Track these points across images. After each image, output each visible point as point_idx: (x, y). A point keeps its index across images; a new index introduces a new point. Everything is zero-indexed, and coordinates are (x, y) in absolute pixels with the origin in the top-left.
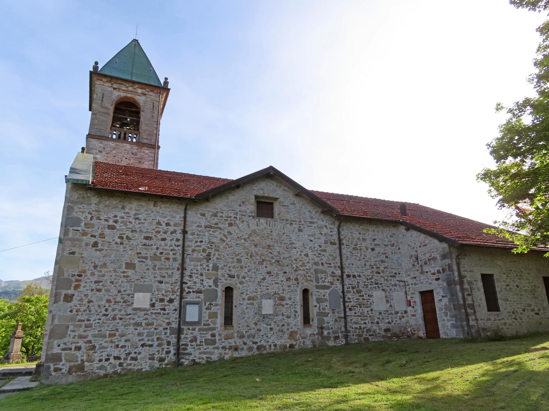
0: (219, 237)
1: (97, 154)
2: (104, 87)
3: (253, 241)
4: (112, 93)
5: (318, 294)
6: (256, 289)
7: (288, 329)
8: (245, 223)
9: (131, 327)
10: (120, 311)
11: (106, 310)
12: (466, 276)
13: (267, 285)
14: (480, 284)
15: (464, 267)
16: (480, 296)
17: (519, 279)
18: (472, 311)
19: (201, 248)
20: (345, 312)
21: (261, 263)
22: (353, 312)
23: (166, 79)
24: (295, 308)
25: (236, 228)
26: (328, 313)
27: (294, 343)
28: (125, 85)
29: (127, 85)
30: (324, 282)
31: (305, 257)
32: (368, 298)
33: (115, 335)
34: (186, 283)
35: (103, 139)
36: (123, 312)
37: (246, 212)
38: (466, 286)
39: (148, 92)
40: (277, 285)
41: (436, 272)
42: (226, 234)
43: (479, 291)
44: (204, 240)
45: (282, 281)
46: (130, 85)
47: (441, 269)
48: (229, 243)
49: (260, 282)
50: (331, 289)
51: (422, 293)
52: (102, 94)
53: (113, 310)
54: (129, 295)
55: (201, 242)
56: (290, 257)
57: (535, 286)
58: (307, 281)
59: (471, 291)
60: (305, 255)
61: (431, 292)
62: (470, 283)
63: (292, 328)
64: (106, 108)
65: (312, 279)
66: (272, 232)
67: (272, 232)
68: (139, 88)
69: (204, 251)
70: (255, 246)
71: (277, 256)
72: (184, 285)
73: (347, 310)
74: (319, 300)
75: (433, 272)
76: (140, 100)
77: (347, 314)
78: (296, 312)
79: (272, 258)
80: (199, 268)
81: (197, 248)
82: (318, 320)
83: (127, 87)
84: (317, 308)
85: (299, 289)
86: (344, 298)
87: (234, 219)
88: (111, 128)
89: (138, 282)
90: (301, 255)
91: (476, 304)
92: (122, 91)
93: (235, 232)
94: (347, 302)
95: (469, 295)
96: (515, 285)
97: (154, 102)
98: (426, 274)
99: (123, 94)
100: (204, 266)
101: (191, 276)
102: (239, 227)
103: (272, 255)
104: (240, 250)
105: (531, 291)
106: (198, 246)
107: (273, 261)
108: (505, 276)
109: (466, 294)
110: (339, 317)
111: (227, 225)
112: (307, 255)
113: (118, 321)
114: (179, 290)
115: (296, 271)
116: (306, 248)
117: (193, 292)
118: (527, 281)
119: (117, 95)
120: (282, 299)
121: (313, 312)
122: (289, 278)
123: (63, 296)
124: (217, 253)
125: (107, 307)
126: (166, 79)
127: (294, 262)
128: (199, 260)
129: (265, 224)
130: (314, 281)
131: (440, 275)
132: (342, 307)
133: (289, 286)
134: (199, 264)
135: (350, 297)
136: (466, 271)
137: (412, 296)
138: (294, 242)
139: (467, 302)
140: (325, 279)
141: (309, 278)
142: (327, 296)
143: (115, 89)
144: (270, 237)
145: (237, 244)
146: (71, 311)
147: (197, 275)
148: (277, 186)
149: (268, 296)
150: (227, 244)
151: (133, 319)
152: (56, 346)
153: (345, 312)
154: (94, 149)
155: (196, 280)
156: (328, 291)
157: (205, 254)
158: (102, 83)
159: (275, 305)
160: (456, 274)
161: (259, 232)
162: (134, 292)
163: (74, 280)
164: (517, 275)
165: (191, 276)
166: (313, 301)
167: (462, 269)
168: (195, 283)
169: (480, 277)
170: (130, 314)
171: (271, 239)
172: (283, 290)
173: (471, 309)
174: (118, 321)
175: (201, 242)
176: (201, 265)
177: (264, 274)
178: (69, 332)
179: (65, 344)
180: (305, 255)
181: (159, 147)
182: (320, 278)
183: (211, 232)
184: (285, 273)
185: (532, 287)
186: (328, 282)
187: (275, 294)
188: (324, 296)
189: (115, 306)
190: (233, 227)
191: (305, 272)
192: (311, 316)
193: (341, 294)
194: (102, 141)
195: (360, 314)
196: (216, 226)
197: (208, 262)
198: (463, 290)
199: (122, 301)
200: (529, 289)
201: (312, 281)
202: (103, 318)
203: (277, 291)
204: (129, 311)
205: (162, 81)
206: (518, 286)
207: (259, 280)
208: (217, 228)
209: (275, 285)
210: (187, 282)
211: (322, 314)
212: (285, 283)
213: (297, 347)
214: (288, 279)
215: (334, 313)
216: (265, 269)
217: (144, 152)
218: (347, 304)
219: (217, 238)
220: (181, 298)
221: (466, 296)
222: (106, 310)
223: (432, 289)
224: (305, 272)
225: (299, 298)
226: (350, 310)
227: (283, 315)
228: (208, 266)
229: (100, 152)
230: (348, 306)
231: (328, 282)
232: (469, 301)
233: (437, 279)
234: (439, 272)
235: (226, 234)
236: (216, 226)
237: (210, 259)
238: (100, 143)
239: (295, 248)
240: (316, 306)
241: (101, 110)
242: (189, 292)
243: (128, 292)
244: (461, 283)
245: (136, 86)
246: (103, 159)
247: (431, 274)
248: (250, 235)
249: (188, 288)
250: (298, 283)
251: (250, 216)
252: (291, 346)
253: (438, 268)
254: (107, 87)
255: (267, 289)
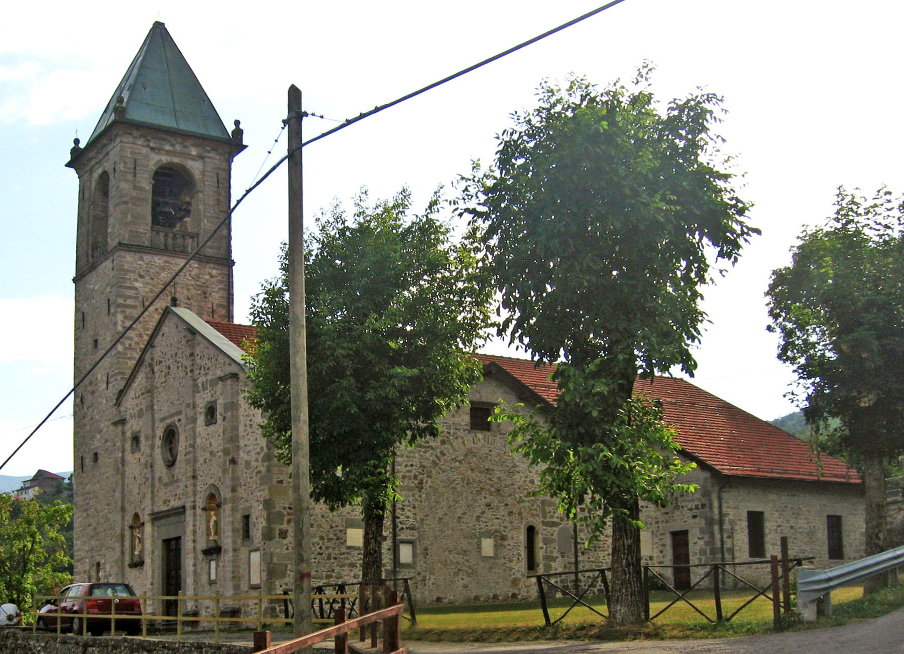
0: (431, 459)
1: (136, 280)
2: (135, 146)
3: (469, 463)
4: (147, 157)
5: (545, 532)
6: (474, 526)
7: (510, 576)
8: (460, 440)
9: (346, 568)
10: (334, 549)
11: (321, 548)
12: (728, 514)
13: (487, 520)
14: (745, 524)
15: (727, 502)
16: (742, 539)
17: (796, 518)
18: (731, 557)
19: (412, 474)
20: (576, 557)
21: (479, 492)
22: (586, 556)
23: (237, 123)
24: (518, 550)
25: (449, 446)
26: (557, 557)
27: (517, 592)
28: (169, 141)
29: (174, 142)
30: (552, 517)
31: (529, 485)
32: (606, 539)
33: (331, 577)
34: (399, 518)
35: (145, 252)
36: (337, 551)
37: (460, 424)
38: (727, 526)
39: (209, 152)
40: (498, 521)
41: (694, 507)
42: (439, 455)
43: (742, 532)
44: (414, 464)
45: (503, 516)
46: (179, 140)
47: (700, 503)
48: (443, 467)
49: (478, 517)
50: (560, 526)
51: (675, 534)
52: (133, 161)
53: (327, 548)
54: (341, 531)
55: (412, 465)
56: (513, 484)
57: (814, 527)
58: (533, 515)
59: (732, 533)
60: (530, 482)
61: (685, 533)
62: (732, 523)
63: (514, 574)
64: (142, 189)
65: (538, 513)
66: (490, 451)
67: (490, 451)
68: (192, 145)
69: (415, 477)
70: (472, 470)
71: (497, 483)
72: (398, 520)
73: (580, 554)
74: (546, 541)
75: (689, 507)
76: (195, 167)
77: (579, 559)
78: (520, 555)
79: (492, 486)
80: (411, 499)
81: (407, 474)
82: (545, 565)
83: (173, 145)
84: (543, 550)
85: (522, 526)
86: (576, 538)
87: (448, 435)
88: (152, 227)
89: (349, 516)
90: (525, 481)
91: (737, 548)
92: (164, 152)
93: (448, 452)
94: (579, 543)
95: (729, 537)
96: (788, 525)
97: (219, 171)
98: (681, 509)
99: (165, 159)
100: (417, 496)
101: (403, 509)
102: (454, 445)
103: (491, 482)
104: (455, 476)
105: (808, 534)
106: (408, 471)
107: (493, 489)
108: (777, 514)
109: (725, 535)
110: (569, 563)
111: (439, 444)
112: (532, 482)
113: (332, 560)
114: (391, 526)
115: (519, 502)
116: (530, 472)
117: (407, 528)
118: (806, 521)
119: (155, 160)
120: (503, 538)
121: (540, 555)
122: (512, 512)
123: (278, 532)
124: (429, 480)
125: (321, 545)
126: (237, 123)
127: (518, 490)
128: (410, 489)
129: (482, 441)
130: (541, 516)
131: (698, 511)
132: (573, 549)
133: (511, 522)
134: (411, 494)
135: (584, 537)
136: (729, 507)
137: (661, 537)
138: (518, 464)
139: (725, 546)
140: (554, 512)
141: (534, 512)
142: (555, 536)
143: (152, 149)
144: (489, 457)
145: (452, 468)
146: (287, 549)
147: (409, 508)
148: (496, 386)
149: (488, 534)
150: (440, 468)
151: (348, 559)
152: (278, 586)
153: (576, 557)
154: (131, 271)
155: (408, 514)
156: (556, 529)
157: (416, 482)
158: (131, 139)
159: (495, 545)
160: (716, 511)
161: (476, 451)
162: (346, 527)
163: (285, 513)
164: (793, 513)
165: (403, 509)
166: (539, 543)
167: (724, 505)
168: (408, 517)
169: (745, 515)
170: (344, 553)
171: (491, 460)
172: (505, 527)
173: (730, 554)
174: (332, 560)
175: (412, 465)
176: (413, 495)
177: (482, 506)
178: (288, 572)
179: (286, 584)
180: (530, 482)
181: (233, 263)
182: (548, 511)
183: (422, 453)
184: (507, 505)
185: (810, 528)
186: (557, 517)
187: (496, 532)
188: (552, 535)
189: (329, 544)
190: (446, 445)
191: (530, 505)
192: (537, 560)
193: (572, 533)
194: (142, 254)
195: (593, 560)
196: (427, 445)
197: (420, 491)
198: (721, 531)
199: (335, 538)
200: (806, 531)
201: (538, 515)
202: (318, 557)
203: (498, 528)
204: (344, 550)
205: (230, 128)
206: (792, 527)
207: (478, 514)
208: (428, 447)
209: (495, 520)
210: (399, 516)
211: (549, 558)
212: (507, 518)
213: (519, 597)
214: (511, 513)
215: (563, 557)
216: (483, 499)
217: (210, 274)
218: (579, 546)
219: (428, 460)
220: (395, 535)
221: (725, 539)
222: (321, 548)
223: (179, 535)
224: (530, 505)
225: (522, 537)
226: (583, 553)
227: (504, 558)
228: (420, 496)
229: (141, 276)
230: (580, 549)
231: (557, 517)
232: (728, 544)
233: (695, 517)
234: (697, 507)
235: (439, 455)
236: (427, 445)
237: (422, 488)
238: (139, 260)
239: (518, 472)
240: (542, 548)
241: (134, 193)
242: (402, 528)
243: (340, 528)
244: (721, 523)
245: (189, 143)
246: (147, 290)
247: (688, 509)
248: (466, 456)
249: (401, 523)
250: (522, 519)
251: (464, 430)
252: (514, 596)
253: (696, 503)
254: (139, 147)
255: (487, 526)
